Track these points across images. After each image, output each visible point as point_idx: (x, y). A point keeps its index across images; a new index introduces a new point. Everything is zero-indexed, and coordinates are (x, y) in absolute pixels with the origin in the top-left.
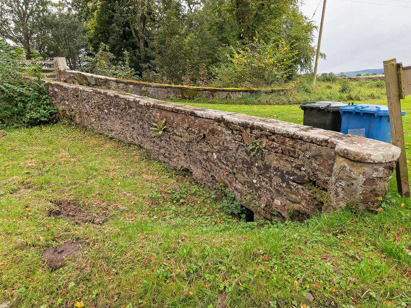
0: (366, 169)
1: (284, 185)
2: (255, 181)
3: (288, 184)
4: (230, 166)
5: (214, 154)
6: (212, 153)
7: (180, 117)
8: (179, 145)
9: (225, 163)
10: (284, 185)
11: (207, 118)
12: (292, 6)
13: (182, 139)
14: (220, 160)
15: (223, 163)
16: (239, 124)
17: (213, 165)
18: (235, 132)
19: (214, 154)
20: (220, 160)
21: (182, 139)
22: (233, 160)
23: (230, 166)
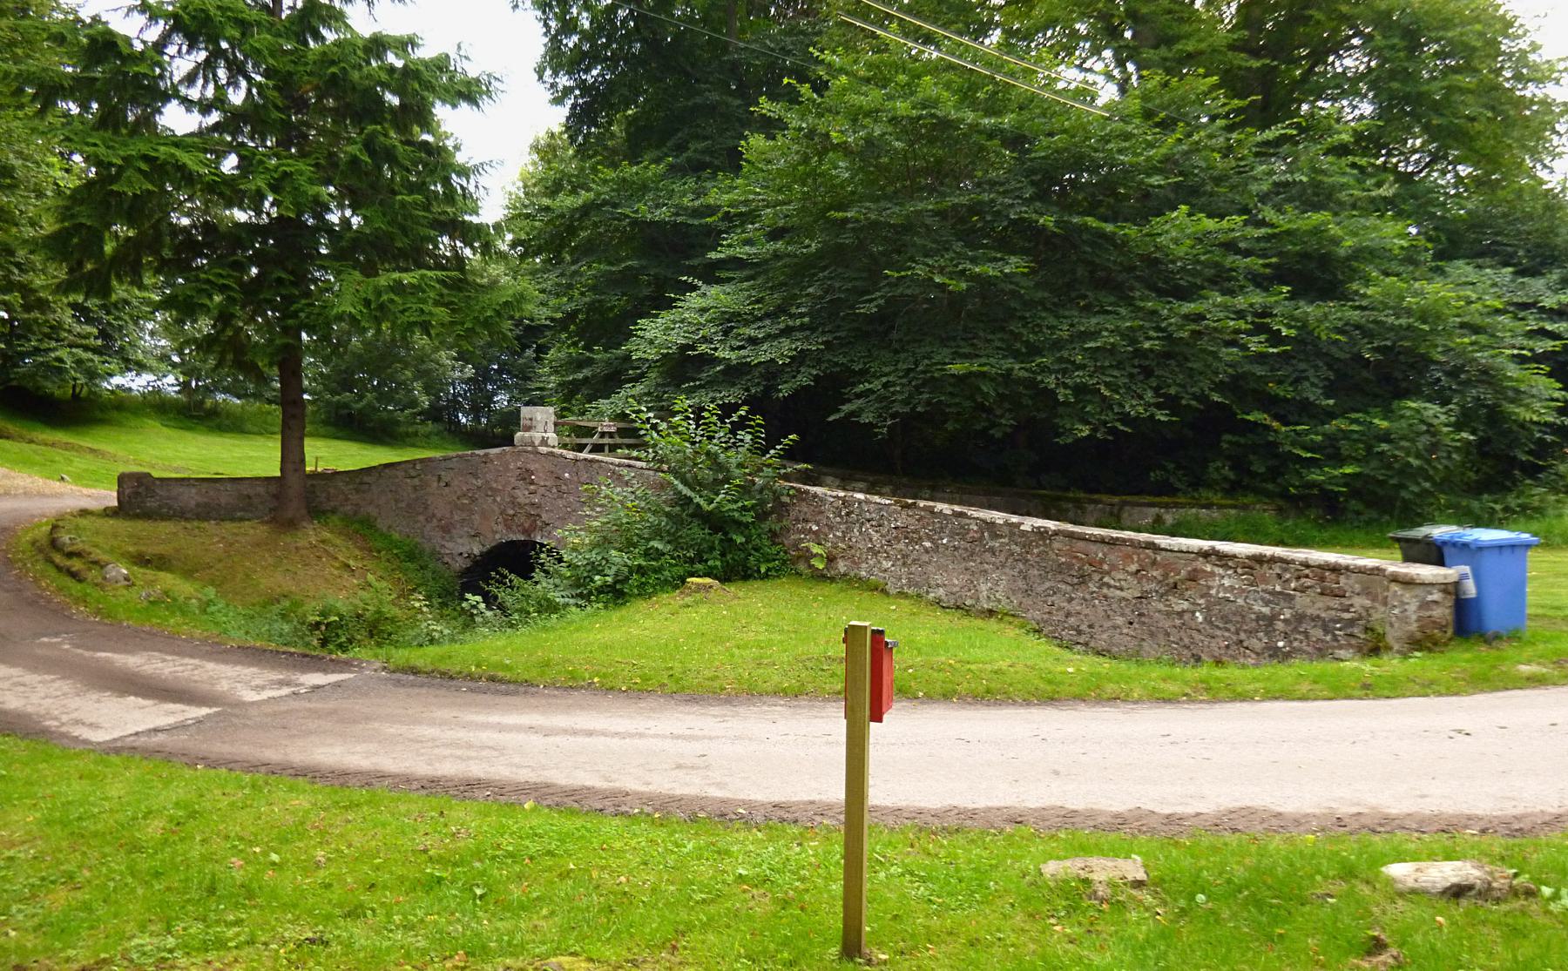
0: (1419, 591)
1: (1328, 638)
2: (1281, 644)
3: (1334, 636)
4: (1233, 629)
5: (1198, 614)
6: (1193, 613)
7: (1102, 641)
8: (1114, 606)
9: (1221, 625)
10: (1328, 638)
11: (1182, 552)
12: (864, 565)
13: (1123, 594)
14: (1211, 623)
15: (1217, 627)
16: (1248, 557)
17: (1195, 634)
18: (1240, 571)
19: (1198, 614)
20: (1211, 623)
21: (1123, 594)
22: (1239, 619)
23: (1233, 629)
